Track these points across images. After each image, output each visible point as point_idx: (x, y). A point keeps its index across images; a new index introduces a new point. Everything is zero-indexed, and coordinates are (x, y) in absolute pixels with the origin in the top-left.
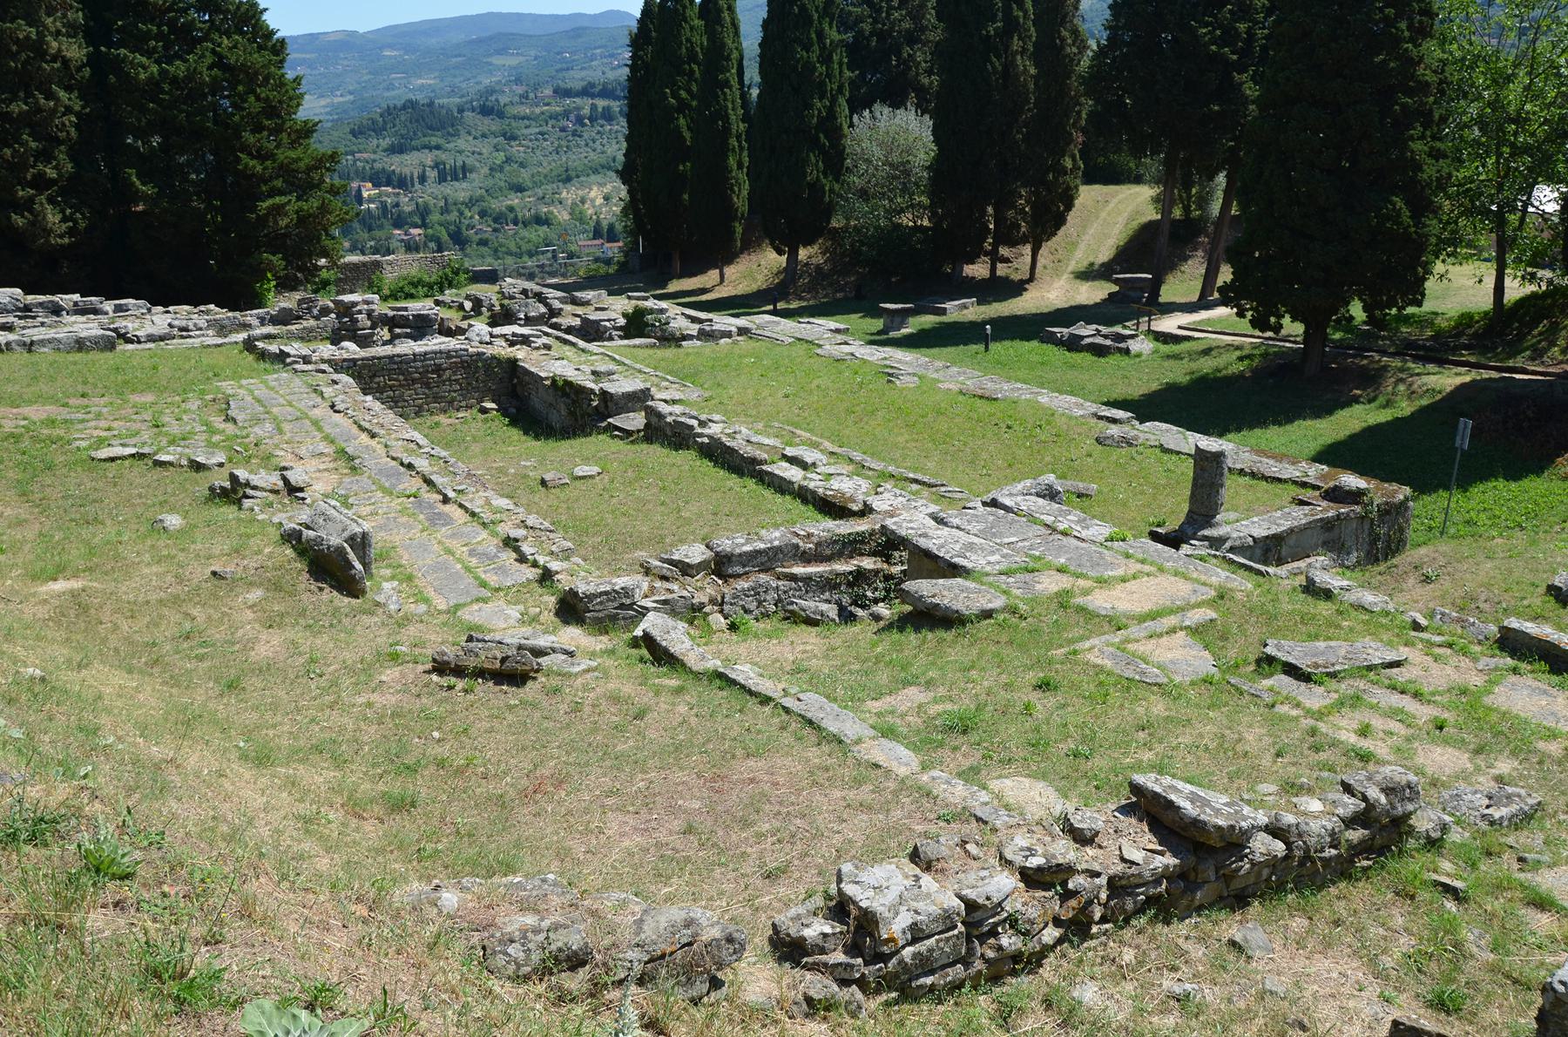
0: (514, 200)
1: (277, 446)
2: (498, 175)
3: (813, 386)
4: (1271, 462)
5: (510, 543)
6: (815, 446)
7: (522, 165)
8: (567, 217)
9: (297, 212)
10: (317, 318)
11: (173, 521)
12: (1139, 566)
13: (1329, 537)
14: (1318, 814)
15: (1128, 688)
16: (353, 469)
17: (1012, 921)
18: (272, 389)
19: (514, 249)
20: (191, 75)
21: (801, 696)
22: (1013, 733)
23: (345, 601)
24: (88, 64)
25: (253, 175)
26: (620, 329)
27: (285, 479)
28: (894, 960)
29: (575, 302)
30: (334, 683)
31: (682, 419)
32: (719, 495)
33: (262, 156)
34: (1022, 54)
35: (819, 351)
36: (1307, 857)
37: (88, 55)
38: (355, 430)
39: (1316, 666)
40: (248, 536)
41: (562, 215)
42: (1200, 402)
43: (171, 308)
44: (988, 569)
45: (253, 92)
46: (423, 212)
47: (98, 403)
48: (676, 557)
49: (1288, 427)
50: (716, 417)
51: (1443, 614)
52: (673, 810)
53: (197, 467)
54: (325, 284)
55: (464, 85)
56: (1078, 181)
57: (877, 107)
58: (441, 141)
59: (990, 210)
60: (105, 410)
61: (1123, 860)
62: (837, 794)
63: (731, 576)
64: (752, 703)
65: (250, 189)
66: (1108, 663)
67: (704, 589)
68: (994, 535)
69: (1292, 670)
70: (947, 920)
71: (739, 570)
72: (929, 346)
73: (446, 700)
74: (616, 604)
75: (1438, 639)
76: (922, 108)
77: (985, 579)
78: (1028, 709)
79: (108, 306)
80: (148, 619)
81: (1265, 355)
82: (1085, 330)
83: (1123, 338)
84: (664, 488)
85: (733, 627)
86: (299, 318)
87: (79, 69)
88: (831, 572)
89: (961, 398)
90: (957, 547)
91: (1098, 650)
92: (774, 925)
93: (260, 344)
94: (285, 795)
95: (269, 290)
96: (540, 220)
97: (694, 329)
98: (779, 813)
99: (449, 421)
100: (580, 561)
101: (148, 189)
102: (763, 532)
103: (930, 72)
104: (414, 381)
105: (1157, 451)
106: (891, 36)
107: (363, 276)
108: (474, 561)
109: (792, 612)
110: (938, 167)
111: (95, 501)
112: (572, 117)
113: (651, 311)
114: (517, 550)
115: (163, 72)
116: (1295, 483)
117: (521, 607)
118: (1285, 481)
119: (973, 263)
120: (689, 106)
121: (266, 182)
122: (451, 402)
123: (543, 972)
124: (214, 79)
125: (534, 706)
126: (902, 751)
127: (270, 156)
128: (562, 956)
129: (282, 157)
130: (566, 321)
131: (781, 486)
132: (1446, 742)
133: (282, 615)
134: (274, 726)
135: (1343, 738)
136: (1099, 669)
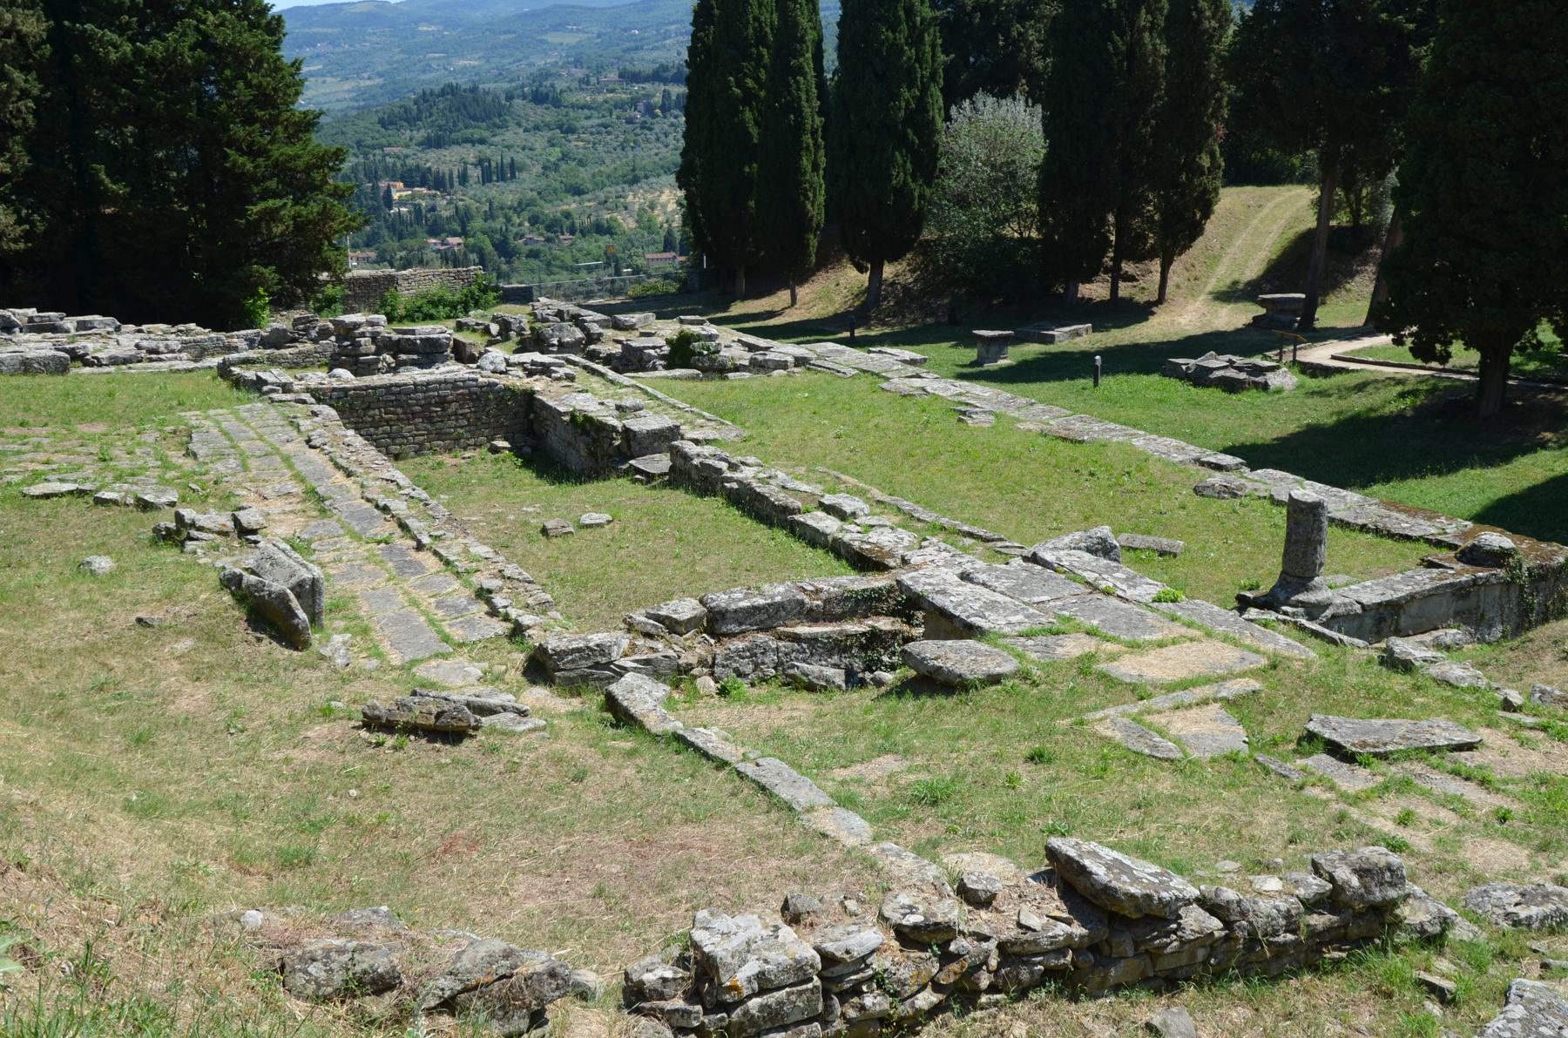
0: (572, 205)
1: (239, 484)
2: (552, 174)
3: (870, 425)
4: (1403, 517)
5: (483, 594)
6: (861, 493)
7: (581, 163)
8: (633, 225)
9: (294, 218)
10: (315, 341)
11: (103, 563)
12: (1183, 630)
13: (1464, 606)
14: (1271, 896)
15: (1135, 763)
16: (323, 511)
17: (879, 980)
18: (242, 420)
19: (569, 261)
20: (172, 56)
21: (760, 761)
22: (986, 807)
23: (282, 653)
24: (49, 40)
25: (243, 174)
26: (662, 357)
27: (236, 521)
28: (738, 1011)
29: (618, 326)
30: (256, 739)
31: (710, 462)
32: (742, 547)
33: (253, 152)
34: (1151, 30)
35: (885, 385)
36: (1253, 940)
37: (48, 30)
38: (330, 468)
39: (1364, 744)
40: (184, 581)
41: (628, 223)
42: (1352, 449)
43: (144, 327)
44: (1007, 630)
45: (244, 77)
46: (464, 217)
47: (38, 434)
48: (663, 612)
49: (1452, 478)
50: (751, 460)
51: (1543, 692)
52: (587, 874)
53: (144, 506)
54: (329, 302)
55: (514, 68)
56: (1218, 183)
57: (980, 96)
58: (486, 134)
59: (1111, 218)
60: (45, 441)
61: (1020, 925)
62: (774, 863)
63: (725, 635)
64: (706, 767)
65: (239, 190)
66: (1118, 736)
67: (693, 649)
68: (1023, 593)
69: (1335, 750)
70: (800, 973)
71: (734, 628)
72: (1028, 381)
73: (372, 757)
74: (590, 663)
75: (1529, 720)
76: (1033, 97)
77: (1000, 641)
78: (1011, 782)
79: (70, 323)
80: (58, 669)
81: (1434, 389)
82: (1214, 361)
83: (1262, 371)
84: (681, 540)
85: (723, 692)
86: (295, 340)
87: (37, 46)
88: (840, 633)
89: (1041, 440)
90: (977, 606)
91: (1110, 722)
92: (626, 974)
93: (236, 370)
94: (163, 845)
95: (263, 308)
96: (601, 229)
97: (744, 357)
98: (702, 880)
99: (454, 461)
100: (558, 615)
101: (120, 189)
102: (766, 587)
103: (1043, 54)
104: (414, 414)
105: (1266, 503)
106: (997, 10)
107: (372, 293)
108: (440, 613)
109: (793, 676)
110: (1050, 170)
111: (22, 542)
112: (641, 106)
113: (699, 338)
114: (489, 602)
115: (137, 53)
116: (1428, 541)
117: (485, 665)
118: (1417, 539)
119: (1090, 282)
120: (756, 97)
121: (257, 182)
122: (457, 440)
123: (346, 993)
124: (197, 60)
125: (467, 765)
126: (856, 821)
127: (263, 152)
128: (367, 978)
129: (276, 154)
130: (606, 348)
131: (814, 539)
132: (1505, 836)
133: (211, 667)
134: (178, 782)
135: (1375, 826)
136: (1106, 741)
